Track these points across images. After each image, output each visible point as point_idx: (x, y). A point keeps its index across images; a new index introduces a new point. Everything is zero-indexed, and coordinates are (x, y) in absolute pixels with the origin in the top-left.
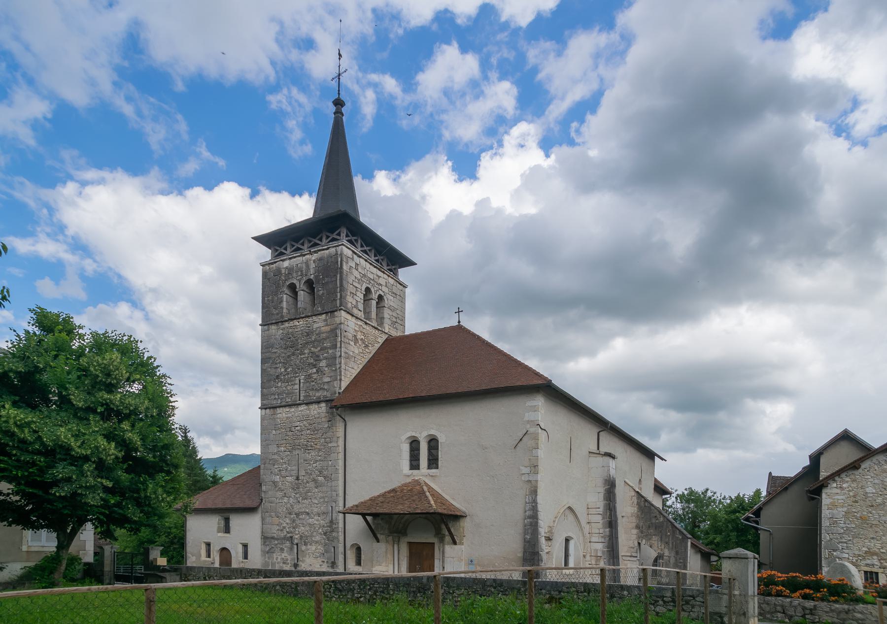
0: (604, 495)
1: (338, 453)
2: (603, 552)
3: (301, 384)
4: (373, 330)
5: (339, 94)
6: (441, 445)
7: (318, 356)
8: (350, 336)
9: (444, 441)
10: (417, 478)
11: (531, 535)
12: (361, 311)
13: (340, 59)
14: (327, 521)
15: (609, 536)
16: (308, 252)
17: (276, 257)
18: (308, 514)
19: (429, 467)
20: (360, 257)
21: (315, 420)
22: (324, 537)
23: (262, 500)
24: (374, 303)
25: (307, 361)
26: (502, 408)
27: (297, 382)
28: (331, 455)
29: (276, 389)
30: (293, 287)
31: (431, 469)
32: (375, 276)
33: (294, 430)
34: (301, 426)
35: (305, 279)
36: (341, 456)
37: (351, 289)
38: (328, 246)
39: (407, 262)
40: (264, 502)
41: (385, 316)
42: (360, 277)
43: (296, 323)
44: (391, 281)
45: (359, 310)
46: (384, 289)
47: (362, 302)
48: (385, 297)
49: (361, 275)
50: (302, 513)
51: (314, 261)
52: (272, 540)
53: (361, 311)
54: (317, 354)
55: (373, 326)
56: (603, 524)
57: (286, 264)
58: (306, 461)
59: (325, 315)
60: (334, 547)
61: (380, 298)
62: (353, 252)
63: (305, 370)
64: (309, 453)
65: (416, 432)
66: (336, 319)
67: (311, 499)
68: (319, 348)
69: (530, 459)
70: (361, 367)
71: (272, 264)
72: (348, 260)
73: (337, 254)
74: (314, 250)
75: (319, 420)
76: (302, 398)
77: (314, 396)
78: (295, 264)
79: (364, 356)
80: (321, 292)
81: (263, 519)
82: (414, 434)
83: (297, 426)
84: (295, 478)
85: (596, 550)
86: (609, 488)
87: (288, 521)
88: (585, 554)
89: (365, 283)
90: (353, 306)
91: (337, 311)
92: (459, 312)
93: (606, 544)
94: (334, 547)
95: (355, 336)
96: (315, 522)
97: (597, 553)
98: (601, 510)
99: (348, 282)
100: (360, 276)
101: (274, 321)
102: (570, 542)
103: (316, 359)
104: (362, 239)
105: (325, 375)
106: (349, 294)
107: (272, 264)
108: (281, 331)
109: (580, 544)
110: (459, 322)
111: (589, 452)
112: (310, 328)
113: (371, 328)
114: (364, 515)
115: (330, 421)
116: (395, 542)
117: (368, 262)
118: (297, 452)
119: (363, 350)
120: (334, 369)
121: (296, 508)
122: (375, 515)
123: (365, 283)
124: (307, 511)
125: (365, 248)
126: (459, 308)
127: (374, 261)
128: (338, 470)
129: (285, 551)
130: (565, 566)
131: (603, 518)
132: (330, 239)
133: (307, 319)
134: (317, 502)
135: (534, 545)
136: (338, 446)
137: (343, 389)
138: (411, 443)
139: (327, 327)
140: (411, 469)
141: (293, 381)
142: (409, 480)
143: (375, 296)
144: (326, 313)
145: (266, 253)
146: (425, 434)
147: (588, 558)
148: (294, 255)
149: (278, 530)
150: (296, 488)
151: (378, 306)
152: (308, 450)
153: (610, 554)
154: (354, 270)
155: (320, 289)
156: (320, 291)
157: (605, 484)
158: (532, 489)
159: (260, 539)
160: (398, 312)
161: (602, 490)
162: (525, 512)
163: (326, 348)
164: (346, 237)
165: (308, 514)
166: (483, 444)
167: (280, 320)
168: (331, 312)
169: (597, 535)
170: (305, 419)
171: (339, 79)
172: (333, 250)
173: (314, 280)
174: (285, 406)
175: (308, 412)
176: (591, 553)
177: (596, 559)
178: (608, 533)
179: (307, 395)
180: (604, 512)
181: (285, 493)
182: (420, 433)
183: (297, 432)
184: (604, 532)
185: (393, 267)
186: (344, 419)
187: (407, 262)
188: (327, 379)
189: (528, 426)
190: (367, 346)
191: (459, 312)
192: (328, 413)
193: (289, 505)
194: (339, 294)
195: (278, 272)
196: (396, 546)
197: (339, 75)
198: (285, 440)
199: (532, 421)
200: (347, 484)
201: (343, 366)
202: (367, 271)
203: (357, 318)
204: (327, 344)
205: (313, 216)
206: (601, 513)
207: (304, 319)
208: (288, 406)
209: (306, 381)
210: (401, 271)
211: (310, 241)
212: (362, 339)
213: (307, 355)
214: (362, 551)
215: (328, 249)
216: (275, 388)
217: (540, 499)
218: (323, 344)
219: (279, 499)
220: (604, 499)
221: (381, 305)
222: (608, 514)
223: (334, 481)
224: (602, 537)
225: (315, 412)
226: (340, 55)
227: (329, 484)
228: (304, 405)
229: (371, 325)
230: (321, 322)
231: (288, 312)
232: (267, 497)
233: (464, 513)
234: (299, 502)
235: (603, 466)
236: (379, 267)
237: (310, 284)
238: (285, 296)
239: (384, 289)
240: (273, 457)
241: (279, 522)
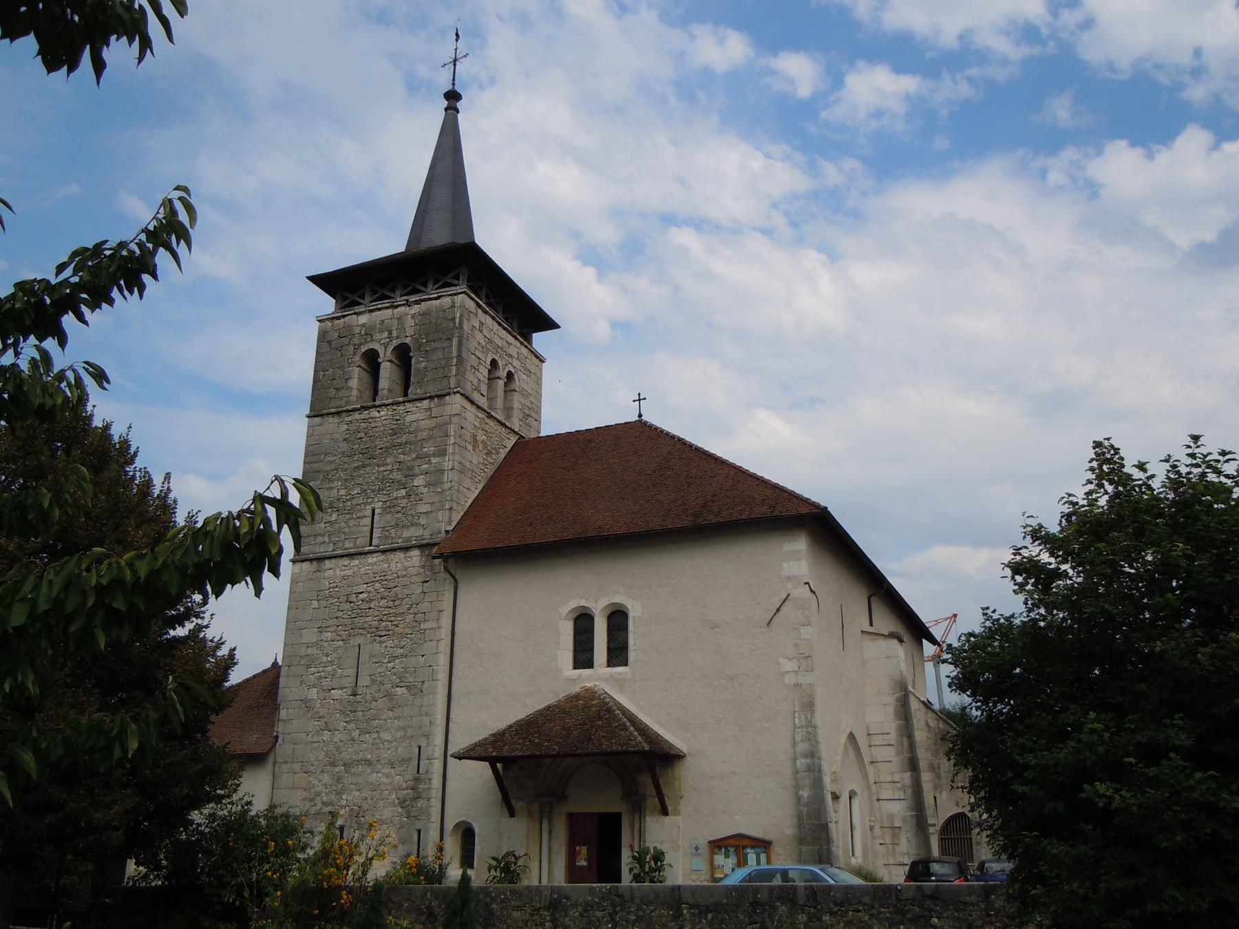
1: (438, 641)
2: (904, 819)
3: (376, 517)
4: (499, 428)
5: (453, 84)
6: (634, 622)
7: (410, 468)
10: (589, 685)
12: (484, 396)
13: (457, 40)
14: (407, 778)
16: (405, 302)
17: (340, 309)
18: (369, 763)
19: (610, 663)
20: (486, 312)
21: (397, 580)
22: (400, 810)
23: (277, 738)
24: (501, 383)
25: (391, 476)
26: (743, 556)
27: (369, 513)
28: (425, 644)
29: (327, 525)
30: (372, 360)
31: (614, 666)
32: (504, 343)
33: (355, 600)
34: (370, 592)
35: (395, 343)
36: (445, 646)
37: (473, 360)
38: (439, 294)
39: (546, 323)
40: (280, 740)
41: (515, 406)
42: (484, 344)
43: (374, 413)
44: (524, 351)
45: (482, 394)
46: (516, 363)
47: (486, 381)
48: (516, 376)
50: (358, 762)
51: (413, 316)
53: (484, 396)
54: (409, 464)
57: (363, 319)
58: (375, 656)
59: (428, 400)
60: (419, 832)
61: (510, 376)
62: (478, 304)
63: (385, 492)
64: (381, 642)
66: (448, 408)
67: (378, 732)
68: (414, 455)
69: (795, 645)
71: (338, 318)
72: (469, 316)
73: (453, 306)
74: (414, 299)
75: (405, 581)
76: (375, 542)
77: (400, 538)
78: (379, 319)
80: (423, 365)
82: (583, 603)
84: (349, 691)
85: (891, 816)
87: (326, 778)
88: (872, 824)
89: (490, 353)
90: (474, 387)
91: (450, 395)
92: (639, 400)
94: (419, 832)
95: (474, 436)
99: (469, 350)
100: (485, 341)
101: (333, 410)
103: (407, 473)
105: (421, 500)
106: (469, 368)
107: (338, 318)
108: (346, 427)
110: (640, 416)
111: (862, 631)
112: (399, 422)
114: (492, 761)
115: (427, 582)
118: (359, 640)
119: (484, 459)
120: (439, 490)
121: (349, 753)
122: (508, 761)
123: (490, 353)
124: (369, 757)
125: (492, 300)
126: (639, 394)
128: (437, 673)
131: (899, 753)
132: (440, 284)
134: (389, 739)
136: (439, 627)
137: (454, 524)
138: (576, 621)
139: (427, 421)
140: (575, 668)
141: (360, 510)
142: (575, 689)
143: (503, 373)
144: (431, 398)
145: (326, 304)
147: (877, 832)
148: (379, 306)
149: (304, 799)
150: (350, 710)
151: (508, 389)
152: (381, 636)
154: (477, 332)
155: (421, 359)
156: (418, 362)
160: (532, 399)
161: (890, 699)
162: (795, 744)
163: (427, 456)
165: (369, 763)
166: (712, 618)
167: (344, 409)
168: (438, 396)
169: (890, 785)
170: (377, 579)
171: (455, 65)
172: (446, 301)
173: (410, 345)
174: (342, 556)
175: (386, 566)
181: (326, 723)
183: (361, 602)
184: (902, 779)
185: (527, 330)
186: (454, 578)
187: (546, 323)
188: (423, 508)
189: (789, 586)
191: (639, 400)
192: (423, 567)
193: (332, 747)
195: (347, 333)
196: (545, 824)
197: (455, 60)
198: (337, 618)
199: (795, 577)
200: (453, 699)
202: (495, 334)
203: (478, 407)
204: (429, 449)
205: (406, 249)
207: (389, 407)
208: (347, 556)
209: (385, 510)
210: (536, 337)
211: (374, 293)
213: (389, 467)
214: (476, 837)
215: (439, 298)
216: (325, 523)
217: (818, 719)
218: (422, 447)
219: (313, 736)
220: (896, 715)
221: (513, 386)
223: (427, 694)
224: (900, 789)
225: (399, 565)
226: (457, 35)
227: (418, 702)
228: (380, 554)
230: (421, 413)
231: (359, 396)
234: (353, 739)
237: (403, 355)
238: (357, 369)
239: (516, 363)
240: (309, 651)
241: (309, 782)
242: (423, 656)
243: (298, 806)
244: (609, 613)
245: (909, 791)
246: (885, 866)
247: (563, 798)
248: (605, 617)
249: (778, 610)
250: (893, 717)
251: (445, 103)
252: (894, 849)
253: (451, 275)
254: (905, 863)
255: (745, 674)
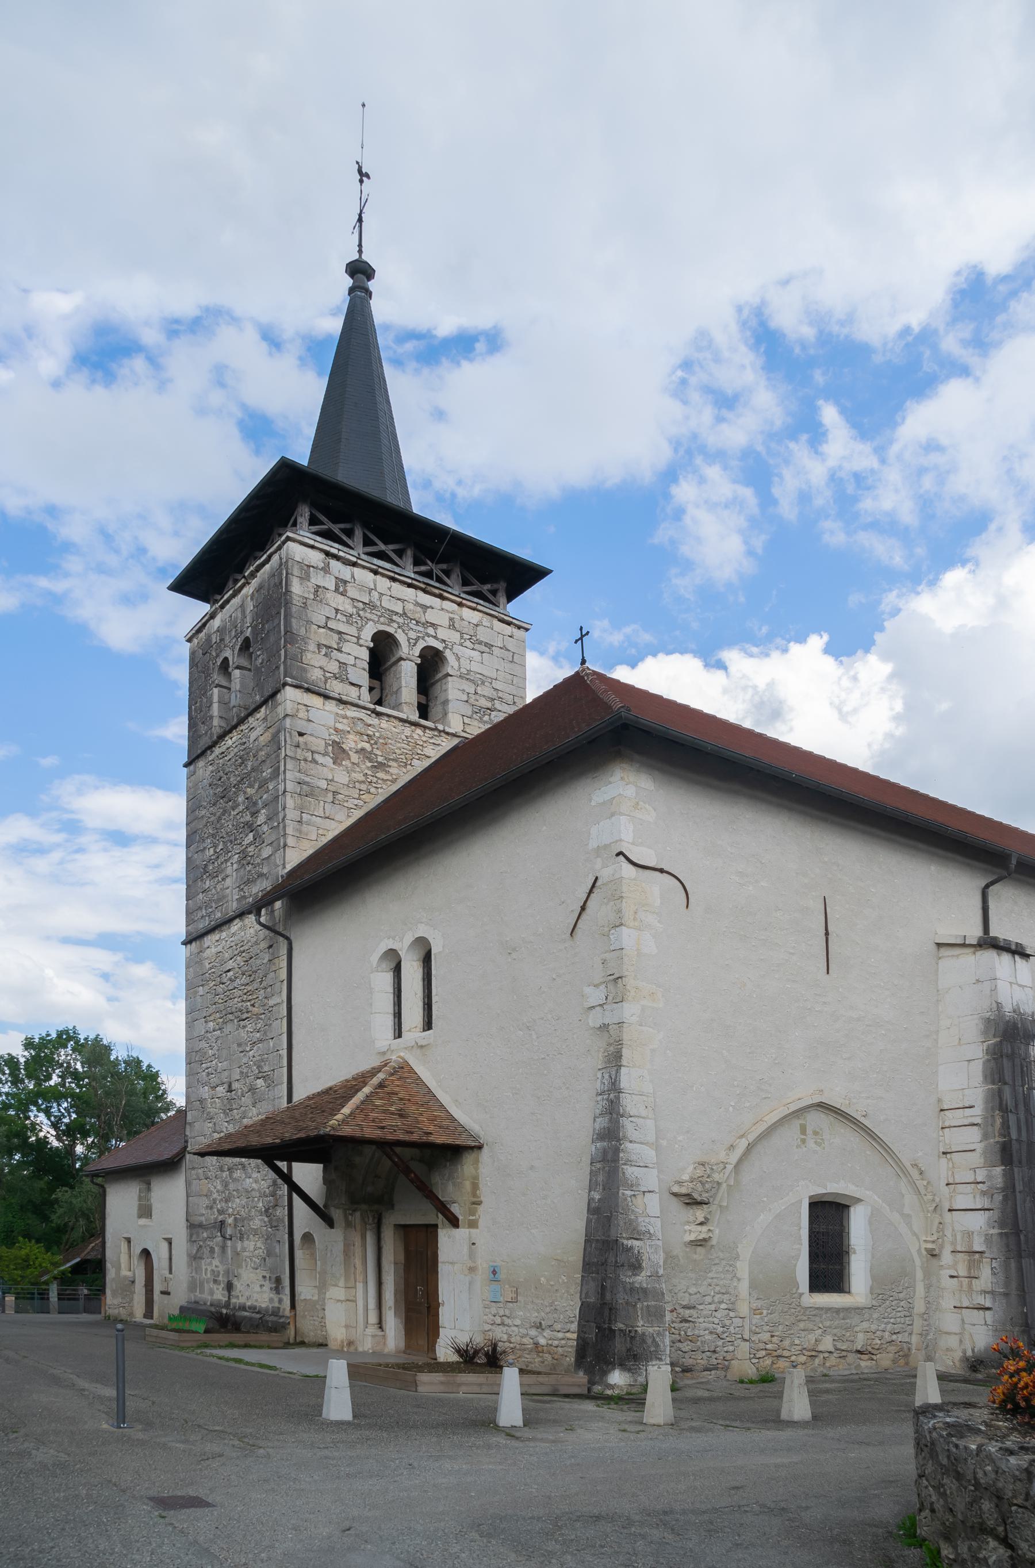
0: (984, 1063)
2: (988, 1239)
5: (360, 251)
8: (319, 745)
9: (441, 950)
11: (604, 1189)
15: (1004, 1189)
41: (450, 697)
48: (448, 654)
49: (361, 605)
52: (201, 1231)
55: (401, 720)
56: (984, 1153)
62: (327, 554)
65: (394, 939)
70: (358, 814)
79: (373, 790)
81: (188, 1184)
83: (229, 971)
85: (969, 1235)
86: (995, 1045)
93: (995, 1215)
96: (254, 1185)
97: (971, 1243)
98: (977, 1114)
99: (309, 622)
102: (852, 1209)
104: (365, 525)
106: (312, 647)
109: (907, 1217)
111: (939, 945)
113: (397, 723)
116: (368, 1227)
117: (383, 575)
127: (413, 575)
129: (216, 1255)
130: (145, 1316)
131: (985, 1136)
133: (241, 728)
135: (609, 1219)
146: (409, 939)
153: (1007, 1246)
157: (985, 1032)
158: (612, 1048)
159: (185, 1229)
160: (497, 685)
164: (310, 524)
176: (953, 1243)
177: (969, 1261)
178: (999, 1181)
179: (242, 897)
180: (985, 1118)
182: (401, 940)
184: (990, 1177)
185: (488, 587)
189: (599, 863)
190: (381, 766)
194: (283, 652)
201: (292, 814)
203: (341, 701)
206: (978, 1120)
212: (363, 750)
220: (985, 1077)
222: (999, 1121)
224: (984, 1193)
229: (395, 718)
232: (193, 1135)
233: (475, 1138)
235: (978, 981)
236: (423, 586)
241: (209, 1190)
242: (272, 1038)
243: (204, 1215)
244: (424, 954)
245: (999, 1197)
246: (956, 1310)
247: (391, 1206)
248: (418, 960)
249: (583, 908)
250: (981, 1078)
251: (349, 282)
252: (970, 1285)
253: (342, 526)
254: (987, 1306)
255: (542, 1019)
